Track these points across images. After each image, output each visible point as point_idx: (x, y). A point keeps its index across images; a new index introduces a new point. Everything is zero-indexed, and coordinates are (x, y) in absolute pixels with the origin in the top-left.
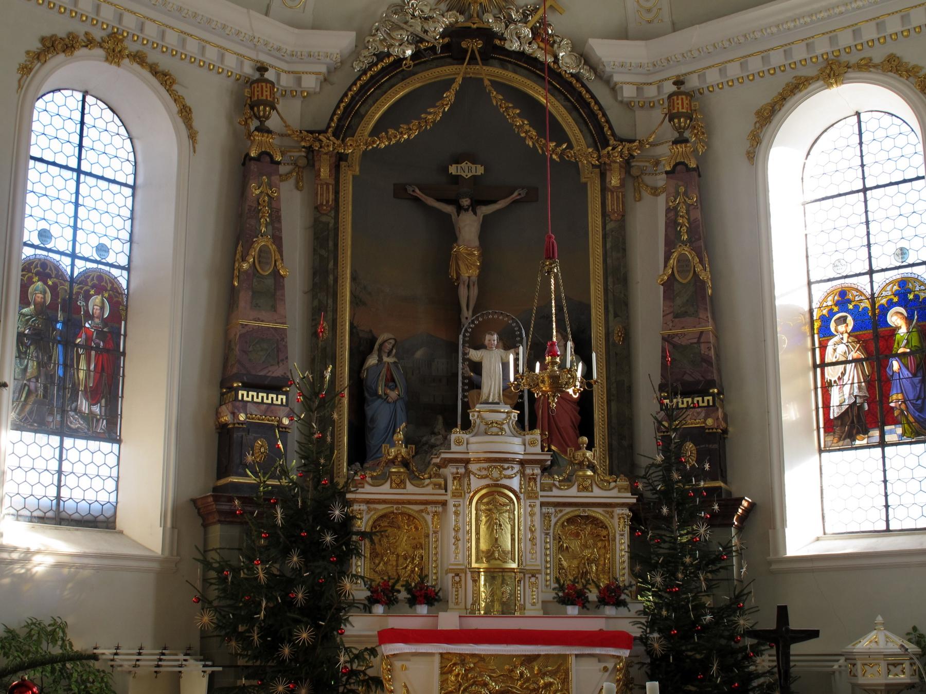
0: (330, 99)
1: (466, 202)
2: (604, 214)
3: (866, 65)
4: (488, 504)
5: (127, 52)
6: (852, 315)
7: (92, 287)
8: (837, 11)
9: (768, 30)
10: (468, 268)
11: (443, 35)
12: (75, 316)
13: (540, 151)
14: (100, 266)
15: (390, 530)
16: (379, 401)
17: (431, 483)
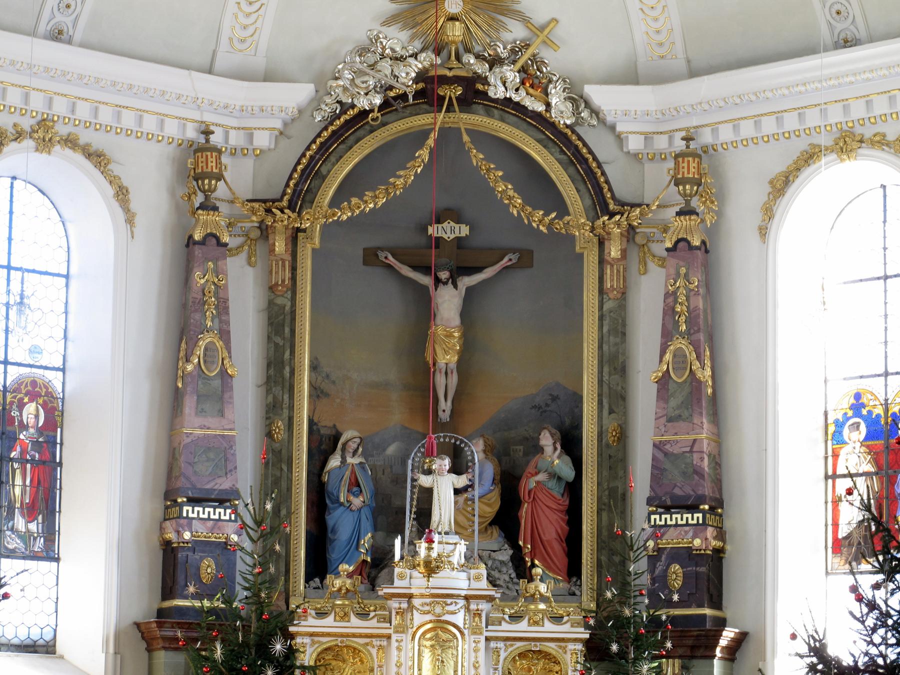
0: (289, 155)
1: (444, 275)
2: (601, 291)
3: (879, 142)
4: (431, 639)
5: (58, 138)
6: (865, 421)
7: (26, 395)
8: (848, 80)
9: (779, 92)
10: (446, 353)
11: (416, 81)
12: (9, 428)
13: (526, 221)
14: (34, 370)
15: (334, 663)
16: (342, 508)
17: (376, 615)
